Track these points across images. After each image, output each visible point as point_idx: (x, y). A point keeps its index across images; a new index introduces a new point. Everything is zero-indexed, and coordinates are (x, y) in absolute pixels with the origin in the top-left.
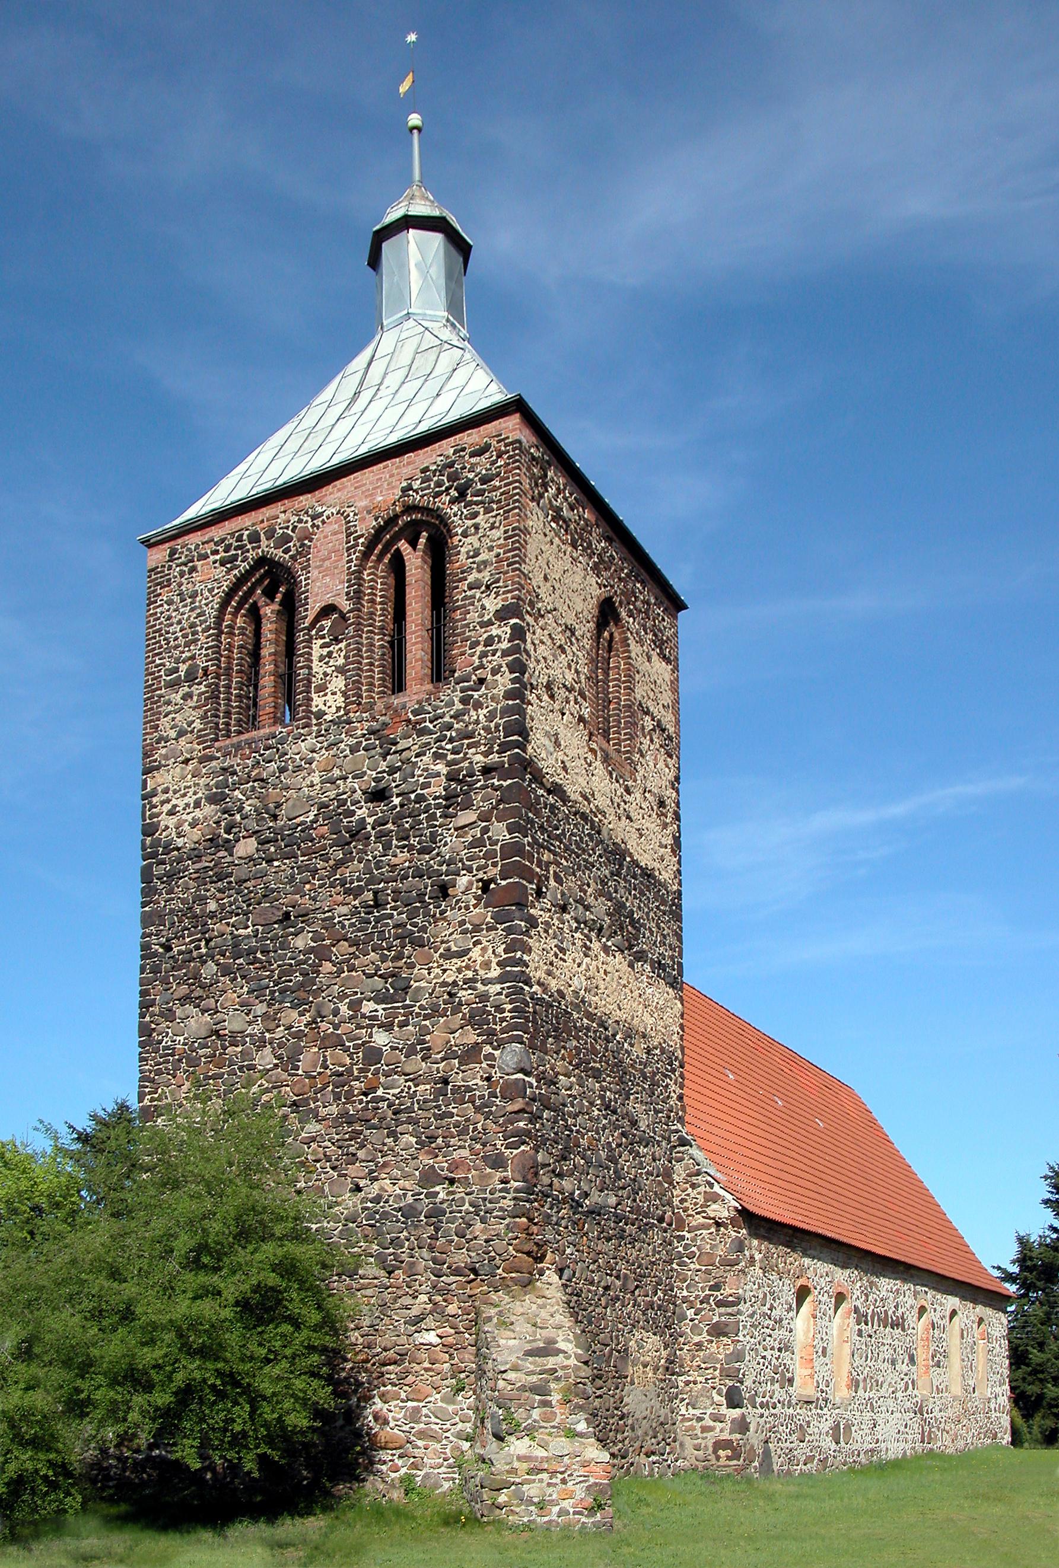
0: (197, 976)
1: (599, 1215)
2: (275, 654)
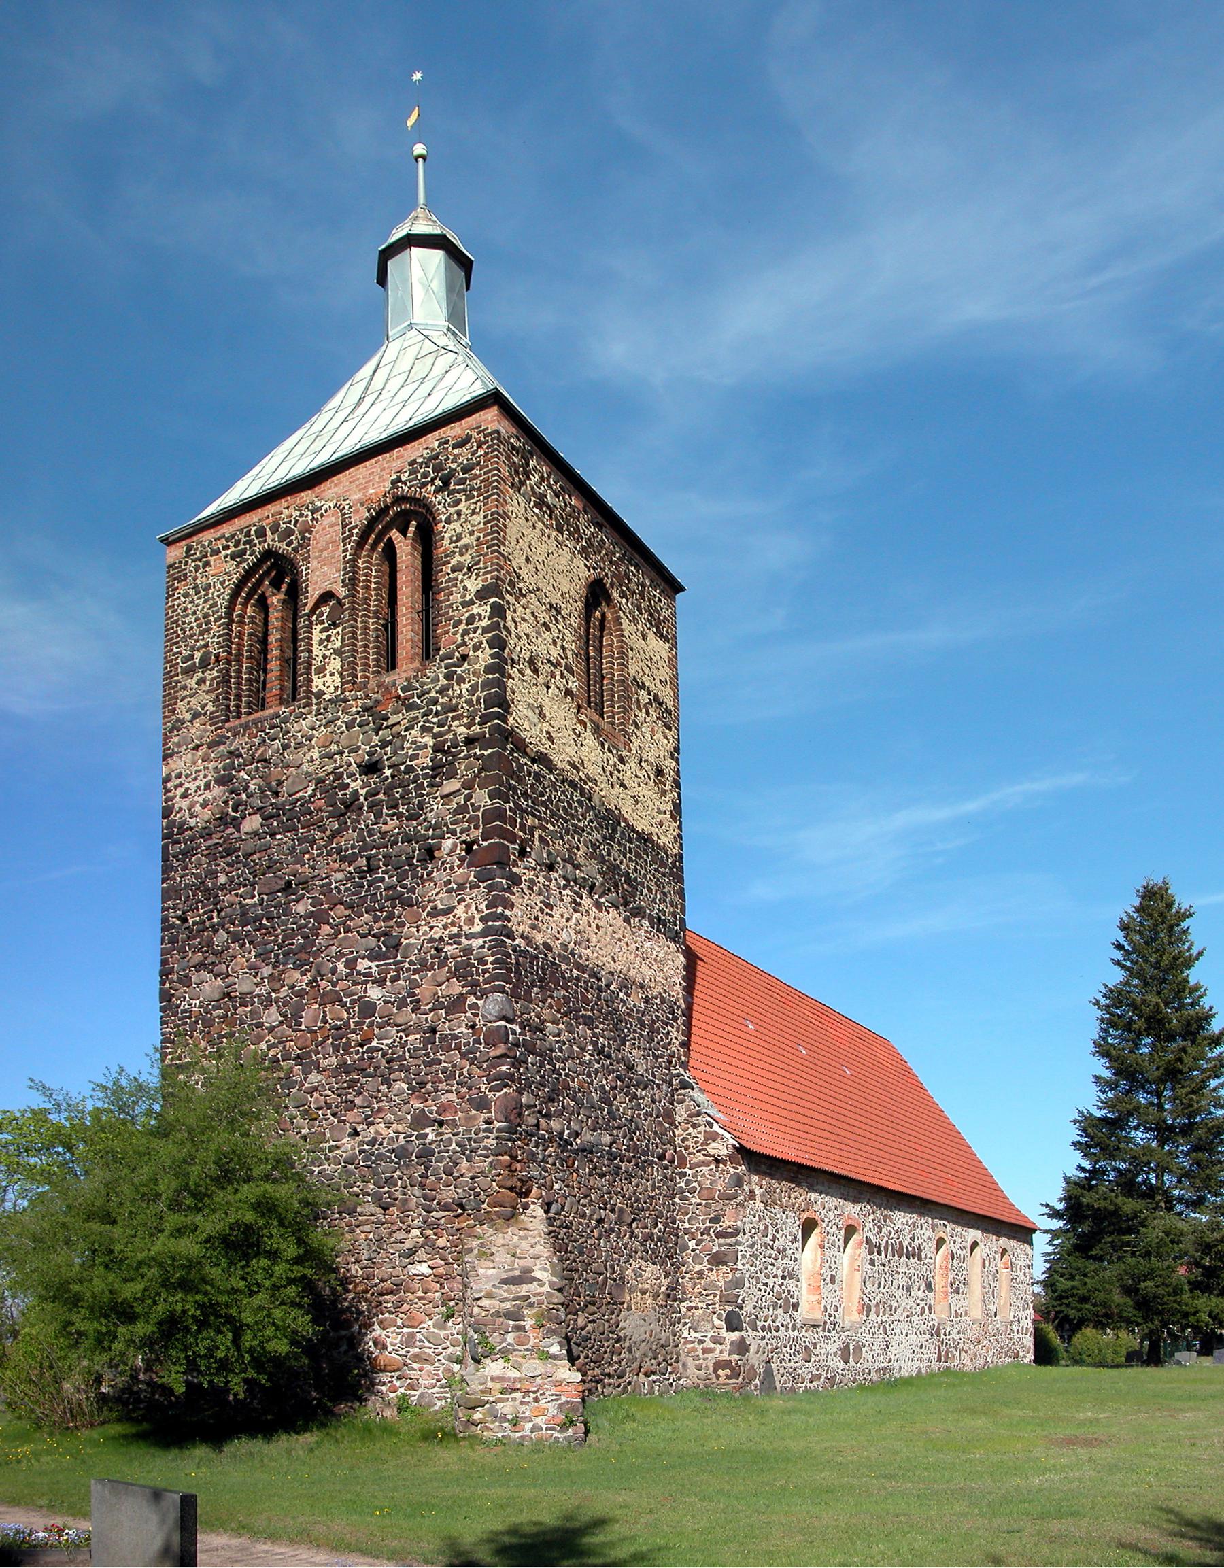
0: (210, 944)
1: (591, 1152)
2: (281, 640)
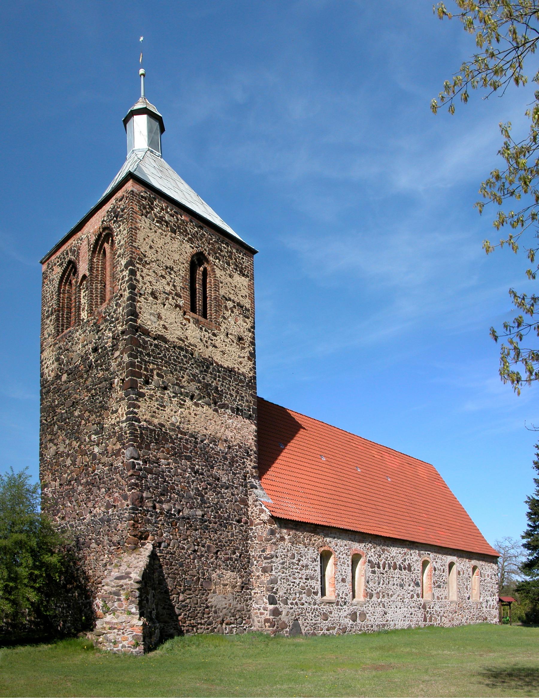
1: (189, 519)
